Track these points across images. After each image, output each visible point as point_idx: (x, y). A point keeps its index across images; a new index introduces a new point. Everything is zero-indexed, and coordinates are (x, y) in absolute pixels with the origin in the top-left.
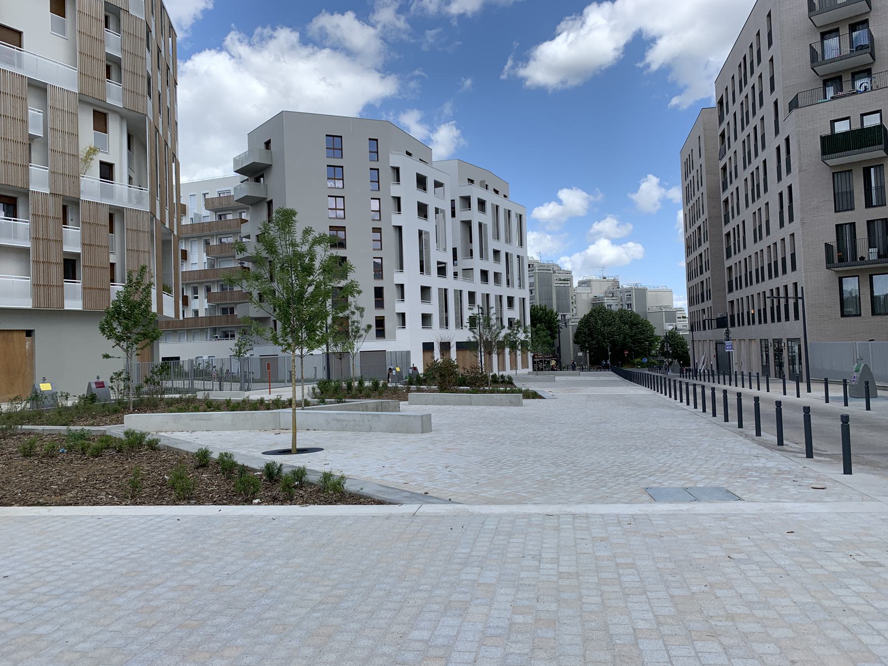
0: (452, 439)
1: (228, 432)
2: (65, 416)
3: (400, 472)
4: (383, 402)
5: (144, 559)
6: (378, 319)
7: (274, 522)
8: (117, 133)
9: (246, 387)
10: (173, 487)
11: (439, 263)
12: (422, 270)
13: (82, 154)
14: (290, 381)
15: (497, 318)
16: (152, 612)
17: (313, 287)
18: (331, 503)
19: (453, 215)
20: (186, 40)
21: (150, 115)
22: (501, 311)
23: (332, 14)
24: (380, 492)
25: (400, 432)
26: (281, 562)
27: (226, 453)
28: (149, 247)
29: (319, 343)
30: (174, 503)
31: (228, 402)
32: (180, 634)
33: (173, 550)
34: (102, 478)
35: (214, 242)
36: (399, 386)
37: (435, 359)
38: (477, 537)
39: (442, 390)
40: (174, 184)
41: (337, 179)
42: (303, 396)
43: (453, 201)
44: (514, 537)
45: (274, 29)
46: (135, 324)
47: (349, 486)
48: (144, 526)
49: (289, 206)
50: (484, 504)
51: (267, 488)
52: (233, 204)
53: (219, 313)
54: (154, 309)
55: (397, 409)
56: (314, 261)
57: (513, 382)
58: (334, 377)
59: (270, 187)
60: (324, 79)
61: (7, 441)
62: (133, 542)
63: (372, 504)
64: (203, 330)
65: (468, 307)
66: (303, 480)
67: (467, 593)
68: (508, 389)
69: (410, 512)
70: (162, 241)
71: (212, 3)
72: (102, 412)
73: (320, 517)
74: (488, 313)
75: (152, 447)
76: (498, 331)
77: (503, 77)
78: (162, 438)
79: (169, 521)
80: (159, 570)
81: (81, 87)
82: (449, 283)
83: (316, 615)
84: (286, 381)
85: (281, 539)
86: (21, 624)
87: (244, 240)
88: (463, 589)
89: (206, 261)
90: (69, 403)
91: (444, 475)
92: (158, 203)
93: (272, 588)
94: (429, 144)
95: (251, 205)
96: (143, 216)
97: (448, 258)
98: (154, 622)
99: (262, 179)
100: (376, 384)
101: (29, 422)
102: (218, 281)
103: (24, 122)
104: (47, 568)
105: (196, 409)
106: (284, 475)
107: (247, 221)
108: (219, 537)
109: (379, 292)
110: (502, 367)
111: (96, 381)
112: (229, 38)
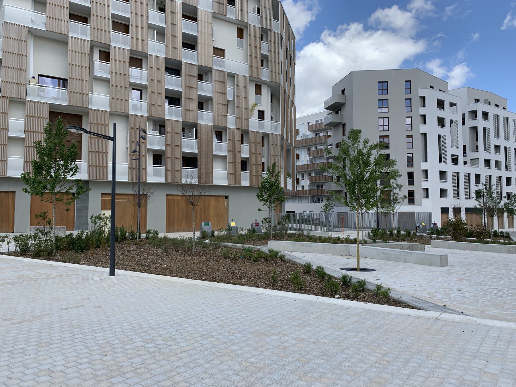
0: (463, 272)
1: (321, 255)
2: (242, 239)
3: (426, 290)
4: (414, 245)
5: (279, 320)
6: (409, 192)
7: (348, 310)
8: (266, 93)
9: (330, 230)
10: (293, 282)
11: (452, 155)
12: (440, 160)
13: (250, 108)
14: (355, 227)
15: (498, 193)
16: (284, 349)
17: (369, 173)
18: (381, 304)
19: (464, 123)
20: (301, 39)
21: (282, 83)
22: (501, 187)
23: (384, 9)
24: (413, 301)
25: (425, 264)
26: (352, 334)
27: (320, 267)
28: (280, 153)
29: (373, 206)
30: (293, 291)
31: (320, 238)
32: (298, 364)
33: (293, 317)
34: (259, 273)
35: (313, 149)
36: (424, 235)
37: (450, 219)
38: (484, 340)
39: (455, 239)
40: (293, 118)
41: (384, 107)
42: (363, 237)
43: (463, 115)
44: (512, 344)
45: (348, 25)
46: (273, 193)
47: (393, 295)
48: (279, 302)
49: (355, 128)
50: (488, 318)
51: (343, 289)
52: (323, 127)
53: (315, 188)
54: (282, 185)
55: (423, 249)
56: (370, 157)
57: (511, 236)
58: (381, 227)
59: (345, 115)
60: (378, 49)
61: (217, 250)
62: (274, 310)
63: (407, 308)
64: (306, 197)
65: (475, 184)
66: (364, 287)
67: (476, 376)
68: (506, 241)
69: (434, 316)
70: (287, 150)
71: (315, 17)
72: (258, 238)
73: (375, 311)
74: (491, 188)
75: (282, 259)
76: (498, 201)
77: (503, 28)
78: (287, 255)
79: (291, 301)
80: (287, 327)
81: (250, 72)
82: (461, 168)
83: (374, 369)
84: (352, 228)
85: (352, 320)
86: (224, 343)
87: (329, 147)
88: (473, 373)
89: (308, 159)
90: (243, 233)
91: (457, 296)
92: (285, 129)
93: (347, 348)
94: (446, 80)
95: (333, 127)
96: (278, 137)
97: (459, 152)
98: (285, 355)
99: (340, 112)
100: (408, 233)
101: (226, 241)
102: (315, 170)
103: (225, 94)
104: (235, 316)
105: (303, 240)
106: (353, 283)
107: (331, 136)
108: (317, 314)
109: (411, 175)
110: (501, 225)
111: (255, 222)
112: (323, 34)
